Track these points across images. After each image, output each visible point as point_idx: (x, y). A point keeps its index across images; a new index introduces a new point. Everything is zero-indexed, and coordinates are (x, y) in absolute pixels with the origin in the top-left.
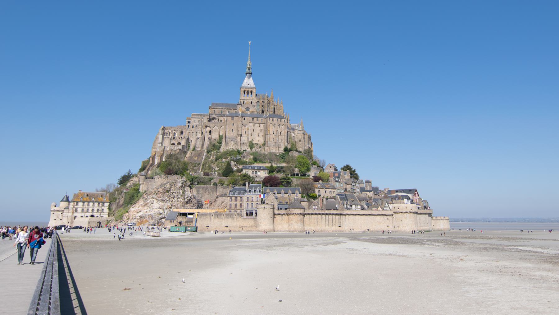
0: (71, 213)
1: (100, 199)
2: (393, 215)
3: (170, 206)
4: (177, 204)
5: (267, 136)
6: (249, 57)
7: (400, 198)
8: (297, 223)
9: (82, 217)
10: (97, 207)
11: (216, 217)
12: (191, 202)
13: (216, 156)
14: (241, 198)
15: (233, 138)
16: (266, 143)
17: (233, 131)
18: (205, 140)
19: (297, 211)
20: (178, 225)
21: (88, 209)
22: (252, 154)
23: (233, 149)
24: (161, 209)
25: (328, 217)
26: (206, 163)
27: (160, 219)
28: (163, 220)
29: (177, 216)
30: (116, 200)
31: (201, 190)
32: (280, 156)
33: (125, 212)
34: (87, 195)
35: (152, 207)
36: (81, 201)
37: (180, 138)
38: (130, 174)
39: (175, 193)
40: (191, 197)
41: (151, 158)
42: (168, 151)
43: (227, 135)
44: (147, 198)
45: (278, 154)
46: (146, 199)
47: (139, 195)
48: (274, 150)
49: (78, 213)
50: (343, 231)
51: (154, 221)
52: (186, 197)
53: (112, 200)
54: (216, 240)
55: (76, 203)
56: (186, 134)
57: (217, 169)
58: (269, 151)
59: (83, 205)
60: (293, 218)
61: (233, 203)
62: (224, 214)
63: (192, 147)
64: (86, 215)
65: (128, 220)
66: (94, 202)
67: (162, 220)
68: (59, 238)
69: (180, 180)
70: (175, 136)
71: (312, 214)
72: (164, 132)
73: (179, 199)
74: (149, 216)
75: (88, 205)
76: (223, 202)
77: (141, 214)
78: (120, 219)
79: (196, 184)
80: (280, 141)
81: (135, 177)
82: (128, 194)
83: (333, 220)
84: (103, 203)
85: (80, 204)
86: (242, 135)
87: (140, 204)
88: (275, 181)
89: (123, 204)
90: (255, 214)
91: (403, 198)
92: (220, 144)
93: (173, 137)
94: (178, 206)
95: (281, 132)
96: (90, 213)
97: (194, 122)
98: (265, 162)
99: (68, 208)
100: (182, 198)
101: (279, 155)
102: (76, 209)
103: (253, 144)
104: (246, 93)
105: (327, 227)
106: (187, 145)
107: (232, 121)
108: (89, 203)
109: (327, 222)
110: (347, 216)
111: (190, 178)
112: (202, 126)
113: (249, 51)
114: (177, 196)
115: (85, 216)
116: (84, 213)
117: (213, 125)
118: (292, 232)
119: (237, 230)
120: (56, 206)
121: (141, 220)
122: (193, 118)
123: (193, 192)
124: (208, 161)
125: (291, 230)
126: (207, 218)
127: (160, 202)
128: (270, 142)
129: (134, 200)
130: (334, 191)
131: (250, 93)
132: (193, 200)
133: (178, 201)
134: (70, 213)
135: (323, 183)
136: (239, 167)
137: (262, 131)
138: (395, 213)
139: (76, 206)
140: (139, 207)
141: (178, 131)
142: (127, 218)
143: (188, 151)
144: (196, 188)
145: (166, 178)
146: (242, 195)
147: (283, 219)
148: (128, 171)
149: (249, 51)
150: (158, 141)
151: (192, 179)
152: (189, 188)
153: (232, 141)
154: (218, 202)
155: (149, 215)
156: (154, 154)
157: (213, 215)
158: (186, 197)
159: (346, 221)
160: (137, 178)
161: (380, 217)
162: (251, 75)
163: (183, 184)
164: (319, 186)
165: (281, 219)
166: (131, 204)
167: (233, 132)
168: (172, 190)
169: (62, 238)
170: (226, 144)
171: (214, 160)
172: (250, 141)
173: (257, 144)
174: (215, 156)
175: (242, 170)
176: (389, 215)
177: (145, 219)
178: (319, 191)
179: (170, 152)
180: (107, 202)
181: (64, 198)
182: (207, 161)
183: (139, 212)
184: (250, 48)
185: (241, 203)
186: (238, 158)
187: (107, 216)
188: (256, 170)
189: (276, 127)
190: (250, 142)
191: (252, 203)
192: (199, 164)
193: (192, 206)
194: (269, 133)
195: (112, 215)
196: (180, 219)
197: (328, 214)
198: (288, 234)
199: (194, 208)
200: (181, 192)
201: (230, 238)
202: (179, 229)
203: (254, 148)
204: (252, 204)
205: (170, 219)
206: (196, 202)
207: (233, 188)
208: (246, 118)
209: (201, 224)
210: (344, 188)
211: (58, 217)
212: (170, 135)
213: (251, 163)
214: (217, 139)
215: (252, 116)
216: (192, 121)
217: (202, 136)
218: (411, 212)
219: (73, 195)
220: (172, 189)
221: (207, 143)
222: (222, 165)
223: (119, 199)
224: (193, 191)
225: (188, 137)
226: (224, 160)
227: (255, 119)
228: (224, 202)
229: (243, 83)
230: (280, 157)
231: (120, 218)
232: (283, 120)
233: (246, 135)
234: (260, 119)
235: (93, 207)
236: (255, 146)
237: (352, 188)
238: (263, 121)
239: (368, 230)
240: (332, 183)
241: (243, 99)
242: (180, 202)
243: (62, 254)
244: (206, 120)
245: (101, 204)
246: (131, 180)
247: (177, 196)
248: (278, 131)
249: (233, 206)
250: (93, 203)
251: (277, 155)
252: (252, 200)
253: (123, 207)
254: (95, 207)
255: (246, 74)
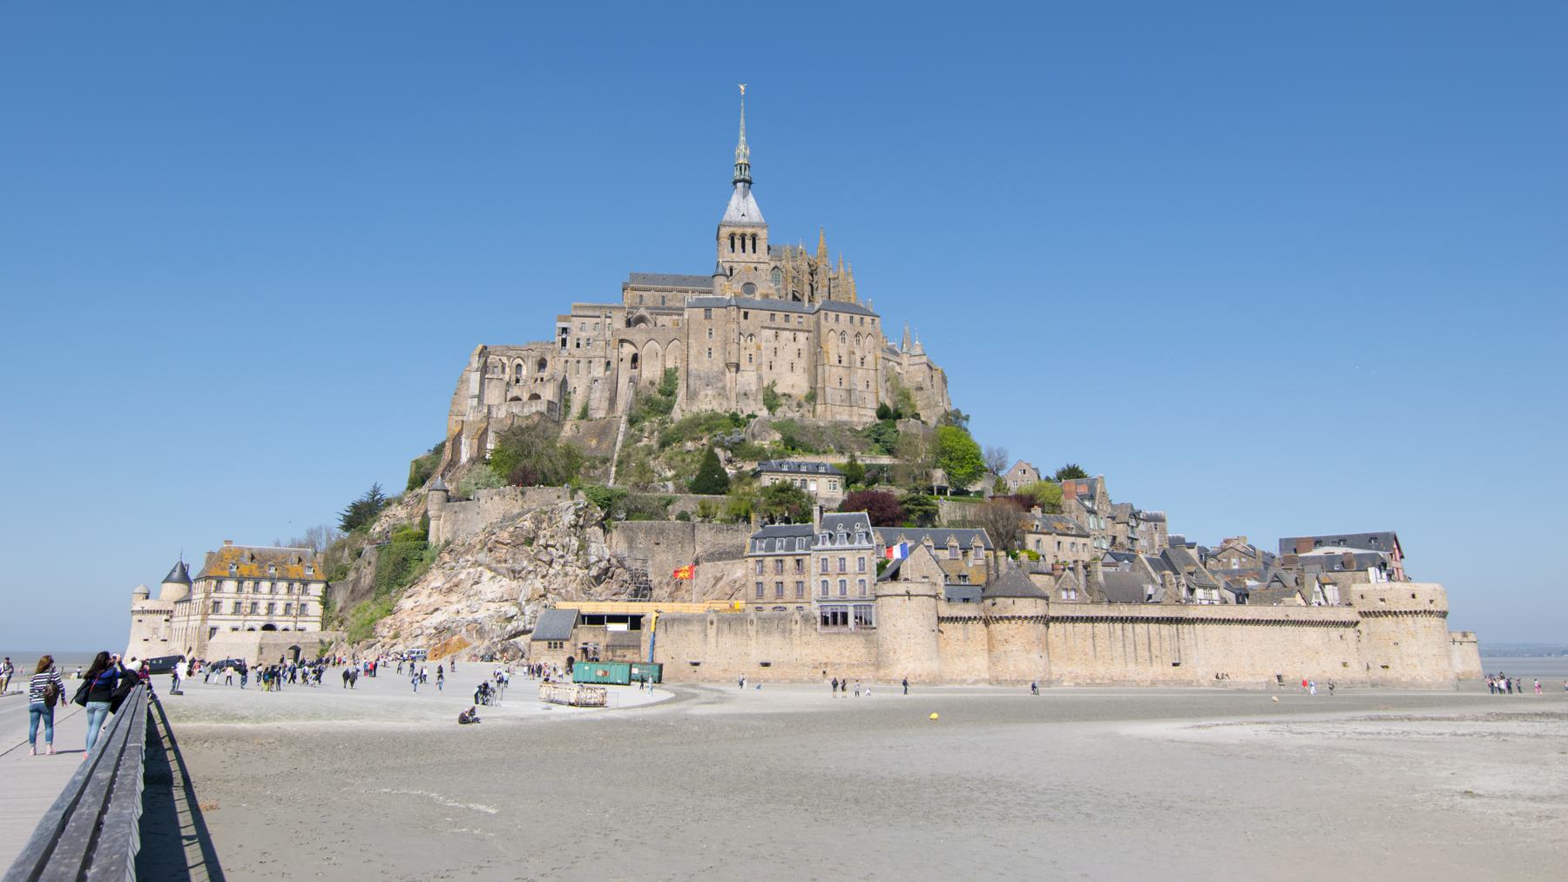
0: (200, 617)
1: (295, 569)
2: (1357, 623)
3: (542, 592)
4: (566, 586)
5: (820, 369)
6: (742, 133)
7: (1350, 563)
8: (1029, 652)
9: (235, 629)
10: (286, 597)
11: (726, 627)
12: (611, 578)
13: (660, 432)
14: (798, 561)
15: (711, 375)
16: (820, 392)
17: (710, 353)
18: (619, 386)
19: (1026, 607)
20: (579, 656)
21: (254, 604)
22: (778, 427)
23: (713, 410)
24: (507, 600)
25: (1134, 630)
26: (629, 455)
27: (510, 637)
28: (522, 641)
29: (575, 627)
30: (346, 574)
31: (641, 535)
32: (866, 433)
33: (383, 613)
34: (253, 558)
35: (475, 594)
36: (231, 577)
37: (536, 380)
38: (378, 497)
39: (553, 546)
40: (609, 560)
41: (447, 444)
42: (501, 420)
43: (691, 366)
44: (454, 564)
45: (860, 429)
46: (453, 568)
47: (426, 554)
48: (843, 415)
49: (223, 617)
50: (1189, 683)
51: (487, 643)
52: (593, 559)
53: (334, 575)
54: (734, 715)
55: (214, 582)
56: (555, 366)
57: (670, 474)
58: (829, 418)
59: (239, 590)
60: (1012, 633)
61: (770, 579)
62: (752, 616)
63: (576, 410)
64: (248, 625)
65: (394, 641)
66: (273, 581)
67: (517, 639)
68: (164, 720)
69: (565, 503)
70: (520, 373)
71: (1074, 620)
72: (486, 361)
73: (568, 569)
74: (470, 627)
75: (256, 590)
76: (718, 580)
77: (437, 618)
78: (367, 637)
79: (621, 516)
80: (861, 387)
81: (395, 505)
82: (389, 552)
83: (1150, 643)
84: (305, 583)
85: (230, 586)
86: (741, 368)
87: (434, 585)
88: (889, 507)
89: (371, 588)
90: (856, 618)
91: (1361, 565)
92: (669, 395)
93: (514, 378)
94: (567, 591)
95: (862, 359)
96: (261, 618)
97: (581, 329)
98: (825, 452)
99: (187, 600)
100: (579, 563)
101: (864, 429)
102: (217, 604)
103: (775, 396)
104: (738, 243)
105: (1131, 666)
106: (560, 401)
107: (707, 322)
108: (257, 583)
109: (1130, 649)
110: (1199, 627)
111: (602, 495)
112: (607, 343)
113: (742, 114)
114: (562, 557)
115: (247, 627)
116: (242, 617)
117: (643, 338)
118: (1010, 687)
119: (805, 679)
120: (147, 598)
121: (443, 642)
122: (576, 316)
123: (614, 544)
124: (634, 450)
125: (1008, 677)
126: (692, 631)
127: (504, 576)
128: (832, 391)
129: (409, 572)
130: (1085, 544)
131: (749, 243)
132: (618, 571)
133: (566, 575)
134: (195, 617)
135: (1044, 517)
136: (741, 467)
137: (804, 354)
138: (1365, 614)
139: (215, 591)
140: (430, 595)
141: (530, 360)
142: (392, 633)
143: (565, 419)
144: (624, 530)
145: (520, 496)
146: (802, 552)
147: (971, 636)
148: (369, 489)
149: (742, 114)
150: (468, 389)
151: (609, 499)
152: (598, 531)
153: (710, 387)
154: (701, 577)
155: (469, 623)
156: (457, 430)
157: (712, 623)
158: (593, 559)
159: (1196, 644)
160: (402, 509)
161: (1315, 629)
162: (749, 188)
163: (579, 516)
164: (1037, 526)
165: (962, 637)
166: (401, 585)
167: (710, 357)
168: (544, 536)
169: (179, 719)
170: (692, 396)
171: (656, 446)
172: (765, 384)
173: (790, 396)
174: (656, 433)
175: (756, 475)
176: (1345, 624)
177: (456, 638)
178: (1038, 541)
179: (509, 422)
180: (318, 581)
181: (174, 570)
182: (631, 450)
183: (432, 613)
184: (742, 104)
185: (798, 578)
186: (736, 438)
187: (317, 626)
188: (804, 477)
189: (847, 340)
190: (768, 388)
191: (842, 577)
192: (605, 461)
193: (614, 592)
194: (826, 361)
195: (336, 623)
196: (586, 635)
197: (1134, 620)
198: (995, 691)
199: (623, 597)
200: (575, 543)
201: (934, 716)
202: (605, 673)
203: (779, 409)
204: (843, 582)
205: (548, 636)
206: (627, 577)
207: (762, 527)
208: (751, 313)
209: (671, 650)
210: (1110, 533)
211: (155, 630)
212: (503, 371)
213: (781, 455)
214: (658, 381)
215: (768, 305)
216: (576, 327)
217: (608, 373)
218: (1431, 613)
219: (205, 556)
220: (541, 533)
221: (625, 393)
222: (684, 460)
223: (357, 569)
224: (614, 541)
225: (565, 376)
226: (689, 445)
227: (780, 316)
228: (721, 578)
229: (727, 212)
230: (869, 436)
231: (365, 634)
232: (868, 319)
233: (754, 368)
234: (794, 316)
235: (270, 597)
236: (783, 401)
237: (1131, 535)
238: (805, 324)
239: (1279, 677)
240: (1074, 515)
241: (730, 260)
242: (572, 578)
243: (184, 832)
244: (618, 322)
245: (297, 585)
246: (383, 513)
247: (562, 557)
248: (854, 353)
249: (770, 590)
250: (272, 584)
251: (858, 432)
252: (860, 569)
253: (373, 595)
254: (277, 597)
255: (735, 183)
